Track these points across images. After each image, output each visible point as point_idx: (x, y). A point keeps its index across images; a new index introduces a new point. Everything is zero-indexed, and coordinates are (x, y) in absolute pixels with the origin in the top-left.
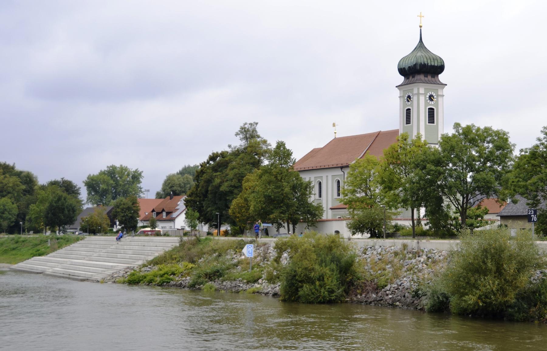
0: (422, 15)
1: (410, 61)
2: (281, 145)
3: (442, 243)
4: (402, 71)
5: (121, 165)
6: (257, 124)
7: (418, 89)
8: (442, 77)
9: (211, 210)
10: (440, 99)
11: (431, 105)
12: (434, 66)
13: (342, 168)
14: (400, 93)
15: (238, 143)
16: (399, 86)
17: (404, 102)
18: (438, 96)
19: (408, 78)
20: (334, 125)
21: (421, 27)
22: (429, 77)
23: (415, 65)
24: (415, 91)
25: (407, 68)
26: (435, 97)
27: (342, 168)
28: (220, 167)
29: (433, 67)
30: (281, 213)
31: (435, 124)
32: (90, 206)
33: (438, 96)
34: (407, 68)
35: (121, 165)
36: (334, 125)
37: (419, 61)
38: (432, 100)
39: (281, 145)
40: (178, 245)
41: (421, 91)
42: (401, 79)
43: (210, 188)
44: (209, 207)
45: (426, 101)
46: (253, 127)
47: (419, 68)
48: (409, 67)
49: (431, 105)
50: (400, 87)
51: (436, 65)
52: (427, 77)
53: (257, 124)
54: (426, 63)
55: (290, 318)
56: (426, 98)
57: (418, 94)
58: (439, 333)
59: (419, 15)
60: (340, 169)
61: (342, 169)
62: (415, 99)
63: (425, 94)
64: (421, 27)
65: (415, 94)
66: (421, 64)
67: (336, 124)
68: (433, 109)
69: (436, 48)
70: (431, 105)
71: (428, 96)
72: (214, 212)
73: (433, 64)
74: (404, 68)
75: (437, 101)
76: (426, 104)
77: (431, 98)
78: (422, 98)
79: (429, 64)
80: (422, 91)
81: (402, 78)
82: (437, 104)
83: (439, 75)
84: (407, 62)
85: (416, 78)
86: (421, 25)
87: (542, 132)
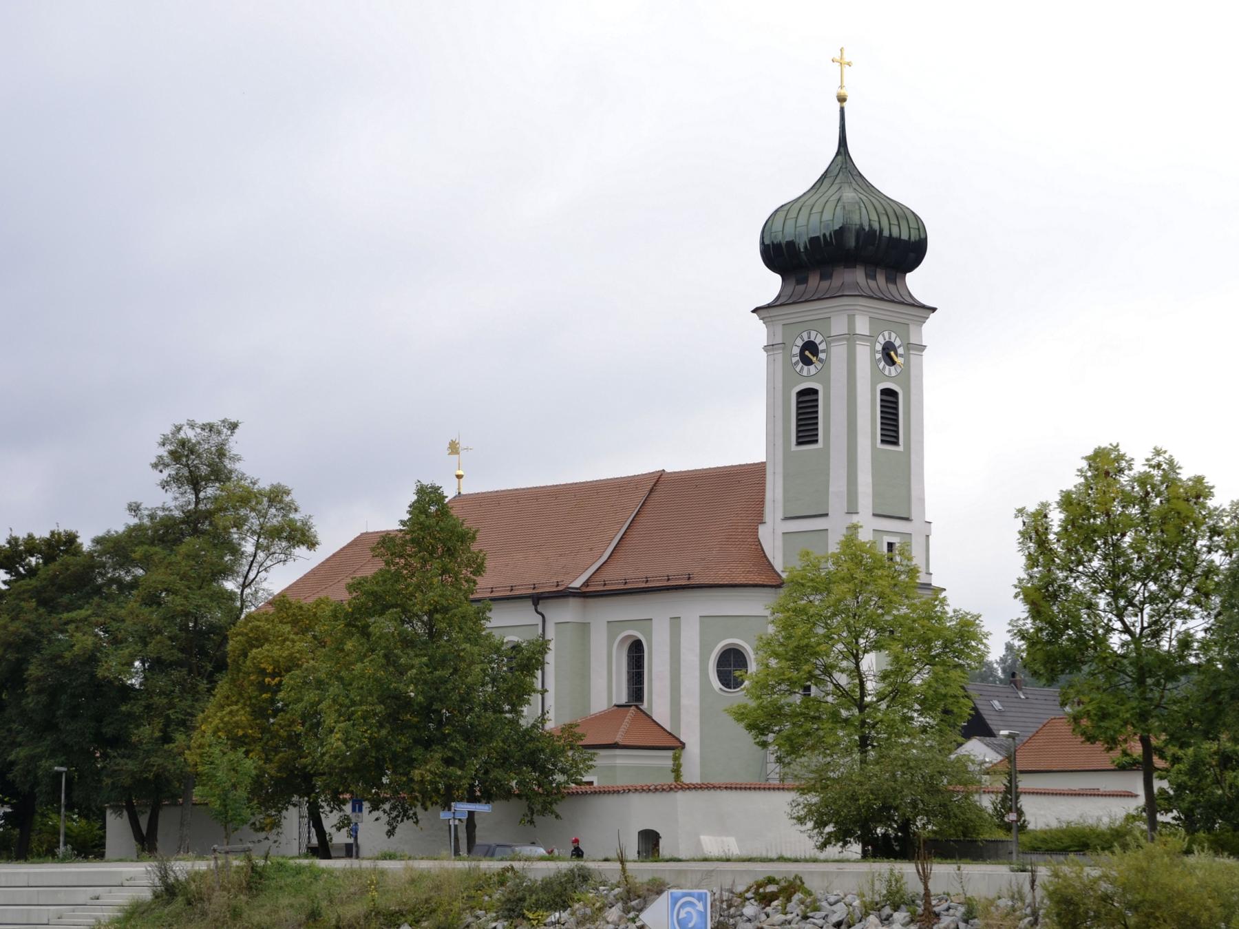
0: (847, 59)
1: (815, 218)
3: (28, 874)
4: (777, 254)
6: (234, 427)
7: (851, 320)
8: (917, 282)
9: (33, 759)
11: (889, 378)
12: (899, 240)
13: (537, 599)
14: (770, 335)
15: (163, 499)
16: (769, 306)
17: (788, 367)
19: (803, 281)
21: (842, 99)
23: (840, 232)
24: (838, 326)
25: (802, 242)
26: (900, 351)
27: (537, 599)
28: (63, 589)
29: (894, 242)
30: (448, 762)
31: (820, 445)
32: (1224, 737)
33: (909, 346)
34: (802, 242)
37: (856, 219)
40: (147, 895)
41: (851, 323)
42: (771, 284)
43: (33, 670)
44: (903, 744)
45: (874, 362)
46: (215, 439)
47: (852, 243)
48: (814, 241)
49: (808, 378)
50: (763, 312)
51: (905, 236)
52: (874, 278)
53: (234, 427)
54: (876, 226)
56: (873, 351)
57: (851, 337)
59: (837, 56)
60: (529, 605)
61: (536, 604)
62: (837, 354)
63: (872, 338)
64: (842, 99)
65: (839, 338)
66: (862, 227)
68: (815, 392)
69: (893, 174)
70: (889, 378)
71: (879, 347)
72: (45, 763)
73: (895, 233)
74: (791, 244)
75: (907, 363)
76: (876, 375)
77: (888, 353)
78: (865, 356)
79: (886, 233)
80: (862, 326)
81: (776, 279)
82: (905, 377)
83: (908, 275)
84: (802, 220)
85: (836, 281)
86: (843, 92)
87: (165, 485)
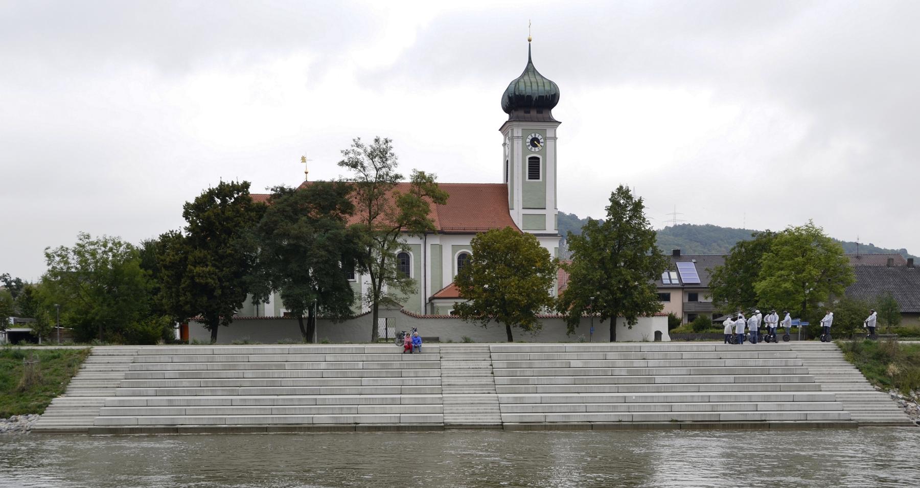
2: (640, 201)
5: (624, 205)
8: (556, 113)
10: (549, 143)
18: (545, 139)
20: (304, 160)
22: (533, 113)
31: (541, 180)
35: (624, 205)
36: (304, 160)
38: (535, 146)
39: (640, 201)
45: (524, 147)
49: (535, 152)
55: (818, 455)
56: (524, 142)
58: (132, 446)
67: (307, 159)
68: (538, 159)
70: (535, 152)
71: (529, 140)
75: (545, 145)
77: (534, 142)
82: (544, 151)
